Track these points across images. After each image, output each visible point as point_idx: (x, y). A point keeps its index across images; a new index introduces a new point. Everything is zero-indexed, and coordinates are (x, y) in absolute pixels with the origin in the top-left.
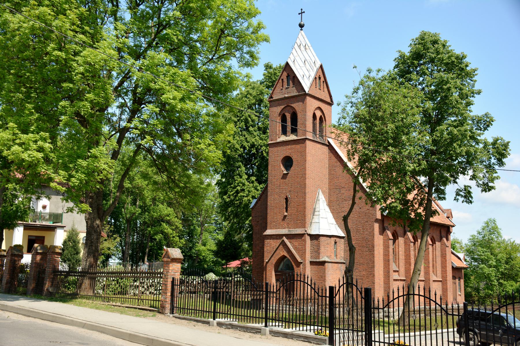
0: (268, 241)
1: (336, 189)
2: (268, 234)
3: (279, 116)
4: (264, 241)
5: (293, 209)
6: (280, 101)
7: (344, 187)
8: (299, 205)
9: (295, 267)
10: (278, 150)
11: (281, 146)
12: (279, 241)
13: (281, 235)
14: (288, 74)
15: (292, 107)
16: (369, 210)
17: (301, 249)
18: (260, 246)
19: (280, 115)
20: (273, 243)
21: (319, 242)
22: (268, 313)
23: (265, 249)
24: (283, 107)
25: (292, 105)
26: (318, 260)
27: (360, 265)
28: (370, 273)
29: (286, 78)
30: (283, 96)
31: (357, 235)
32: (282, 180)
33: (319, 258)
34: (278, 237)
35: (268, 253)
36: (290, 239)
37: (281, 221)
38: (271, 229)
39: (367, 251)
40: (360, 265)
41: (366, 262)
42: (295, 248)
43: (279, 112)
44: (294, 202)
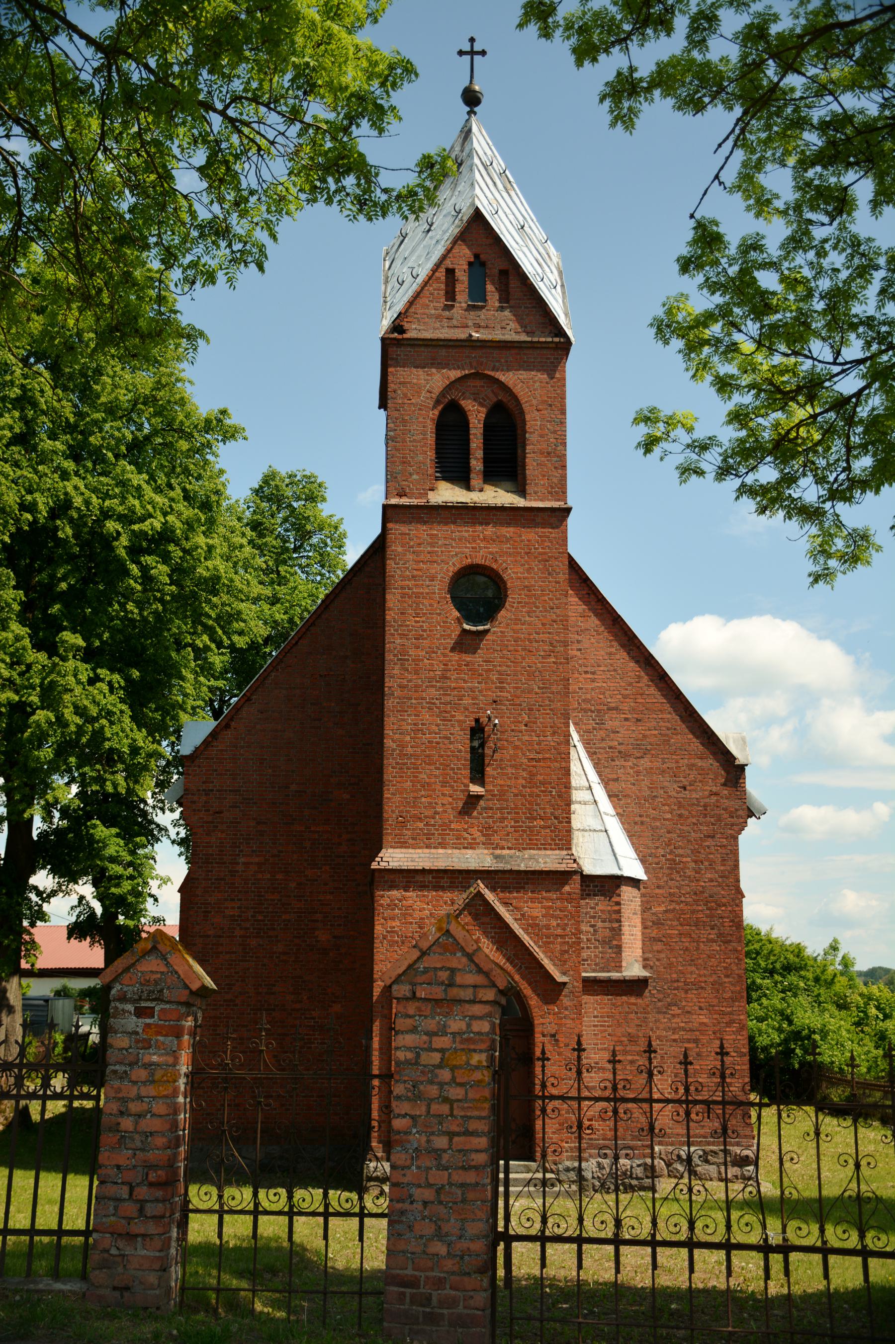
0: (395, 893)
1: (585, 711)
2: (394, 865)
3: (434, 407)
4: (372, 896)
5: (510, 770)
6: (443, 352)
7: (616, 709)
8: (539, 760)
9: (534, 1001)
10: (432, 536)
11: (446, 524)
12: (461, 898)
13: (460, 872)
14: (477, 256)
15: (497, 381)
16: (716, 794)
17: (559, 931)
18: (228, 912)
19: (437, 402)
20: (418, 905)
21: (618, 904)
22: (501, 1203)
23: (378, 929)
24: (455, 374)
25: (502, 377)
26: (615, 975)
27: (686, 992)
28: (726, 1019)
29: (466, 267)
30: (461, 334)
31: (671, 883)
32: (455, 656)
33: (619, 968)
34: (445, 882)
35: (393, 943)
36: (505, 889)
37: (451, 814)
38: (403, 845)
39: (713, 941)
40: (686, 992)
41: (711, 980)
42: (532, 927)
43: (437, 391)
44: (516, 748)
